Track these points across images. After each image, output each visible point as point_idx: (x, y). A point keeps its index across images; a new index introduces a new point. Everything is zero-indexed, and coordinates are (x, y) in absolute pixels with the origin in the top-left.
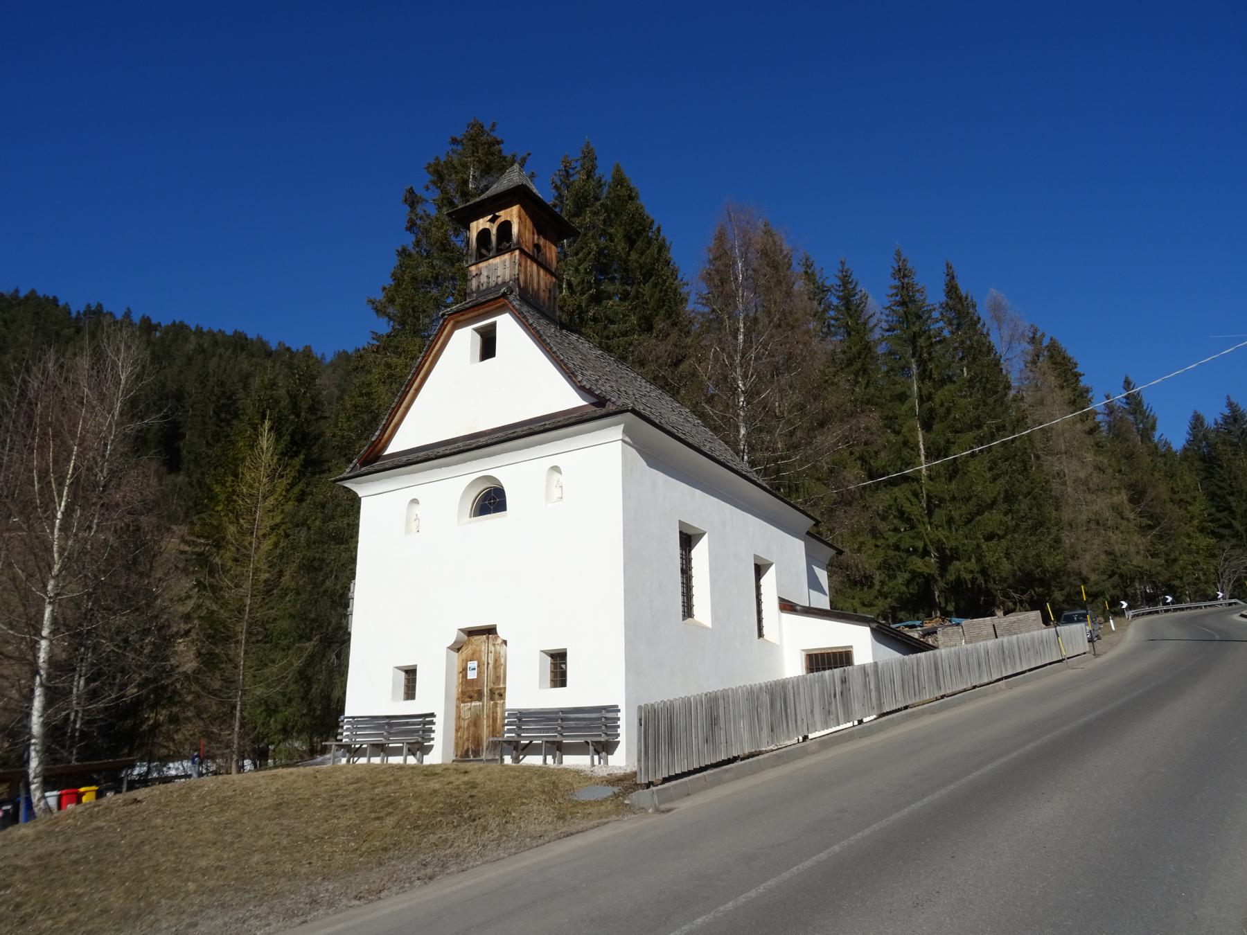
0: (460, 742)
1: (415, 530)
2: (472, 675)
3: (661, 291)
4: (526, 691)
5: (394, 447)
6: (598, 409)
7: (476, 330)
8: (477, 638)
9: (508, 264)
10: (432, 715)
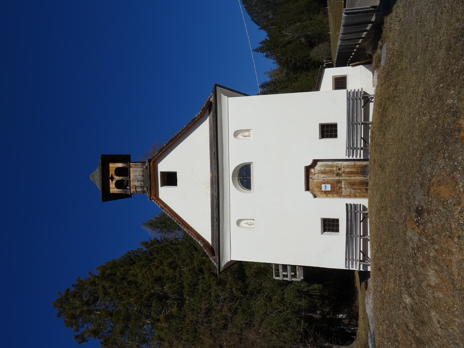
0: (362, 194)
1: (253, 221)
2: (329, 188)
3: (161, 250)
4: (336, 148)
5: (208, 237)
6: (212, 109)
8: (310, 186)
9: (135, 169)
10: (347, 205)
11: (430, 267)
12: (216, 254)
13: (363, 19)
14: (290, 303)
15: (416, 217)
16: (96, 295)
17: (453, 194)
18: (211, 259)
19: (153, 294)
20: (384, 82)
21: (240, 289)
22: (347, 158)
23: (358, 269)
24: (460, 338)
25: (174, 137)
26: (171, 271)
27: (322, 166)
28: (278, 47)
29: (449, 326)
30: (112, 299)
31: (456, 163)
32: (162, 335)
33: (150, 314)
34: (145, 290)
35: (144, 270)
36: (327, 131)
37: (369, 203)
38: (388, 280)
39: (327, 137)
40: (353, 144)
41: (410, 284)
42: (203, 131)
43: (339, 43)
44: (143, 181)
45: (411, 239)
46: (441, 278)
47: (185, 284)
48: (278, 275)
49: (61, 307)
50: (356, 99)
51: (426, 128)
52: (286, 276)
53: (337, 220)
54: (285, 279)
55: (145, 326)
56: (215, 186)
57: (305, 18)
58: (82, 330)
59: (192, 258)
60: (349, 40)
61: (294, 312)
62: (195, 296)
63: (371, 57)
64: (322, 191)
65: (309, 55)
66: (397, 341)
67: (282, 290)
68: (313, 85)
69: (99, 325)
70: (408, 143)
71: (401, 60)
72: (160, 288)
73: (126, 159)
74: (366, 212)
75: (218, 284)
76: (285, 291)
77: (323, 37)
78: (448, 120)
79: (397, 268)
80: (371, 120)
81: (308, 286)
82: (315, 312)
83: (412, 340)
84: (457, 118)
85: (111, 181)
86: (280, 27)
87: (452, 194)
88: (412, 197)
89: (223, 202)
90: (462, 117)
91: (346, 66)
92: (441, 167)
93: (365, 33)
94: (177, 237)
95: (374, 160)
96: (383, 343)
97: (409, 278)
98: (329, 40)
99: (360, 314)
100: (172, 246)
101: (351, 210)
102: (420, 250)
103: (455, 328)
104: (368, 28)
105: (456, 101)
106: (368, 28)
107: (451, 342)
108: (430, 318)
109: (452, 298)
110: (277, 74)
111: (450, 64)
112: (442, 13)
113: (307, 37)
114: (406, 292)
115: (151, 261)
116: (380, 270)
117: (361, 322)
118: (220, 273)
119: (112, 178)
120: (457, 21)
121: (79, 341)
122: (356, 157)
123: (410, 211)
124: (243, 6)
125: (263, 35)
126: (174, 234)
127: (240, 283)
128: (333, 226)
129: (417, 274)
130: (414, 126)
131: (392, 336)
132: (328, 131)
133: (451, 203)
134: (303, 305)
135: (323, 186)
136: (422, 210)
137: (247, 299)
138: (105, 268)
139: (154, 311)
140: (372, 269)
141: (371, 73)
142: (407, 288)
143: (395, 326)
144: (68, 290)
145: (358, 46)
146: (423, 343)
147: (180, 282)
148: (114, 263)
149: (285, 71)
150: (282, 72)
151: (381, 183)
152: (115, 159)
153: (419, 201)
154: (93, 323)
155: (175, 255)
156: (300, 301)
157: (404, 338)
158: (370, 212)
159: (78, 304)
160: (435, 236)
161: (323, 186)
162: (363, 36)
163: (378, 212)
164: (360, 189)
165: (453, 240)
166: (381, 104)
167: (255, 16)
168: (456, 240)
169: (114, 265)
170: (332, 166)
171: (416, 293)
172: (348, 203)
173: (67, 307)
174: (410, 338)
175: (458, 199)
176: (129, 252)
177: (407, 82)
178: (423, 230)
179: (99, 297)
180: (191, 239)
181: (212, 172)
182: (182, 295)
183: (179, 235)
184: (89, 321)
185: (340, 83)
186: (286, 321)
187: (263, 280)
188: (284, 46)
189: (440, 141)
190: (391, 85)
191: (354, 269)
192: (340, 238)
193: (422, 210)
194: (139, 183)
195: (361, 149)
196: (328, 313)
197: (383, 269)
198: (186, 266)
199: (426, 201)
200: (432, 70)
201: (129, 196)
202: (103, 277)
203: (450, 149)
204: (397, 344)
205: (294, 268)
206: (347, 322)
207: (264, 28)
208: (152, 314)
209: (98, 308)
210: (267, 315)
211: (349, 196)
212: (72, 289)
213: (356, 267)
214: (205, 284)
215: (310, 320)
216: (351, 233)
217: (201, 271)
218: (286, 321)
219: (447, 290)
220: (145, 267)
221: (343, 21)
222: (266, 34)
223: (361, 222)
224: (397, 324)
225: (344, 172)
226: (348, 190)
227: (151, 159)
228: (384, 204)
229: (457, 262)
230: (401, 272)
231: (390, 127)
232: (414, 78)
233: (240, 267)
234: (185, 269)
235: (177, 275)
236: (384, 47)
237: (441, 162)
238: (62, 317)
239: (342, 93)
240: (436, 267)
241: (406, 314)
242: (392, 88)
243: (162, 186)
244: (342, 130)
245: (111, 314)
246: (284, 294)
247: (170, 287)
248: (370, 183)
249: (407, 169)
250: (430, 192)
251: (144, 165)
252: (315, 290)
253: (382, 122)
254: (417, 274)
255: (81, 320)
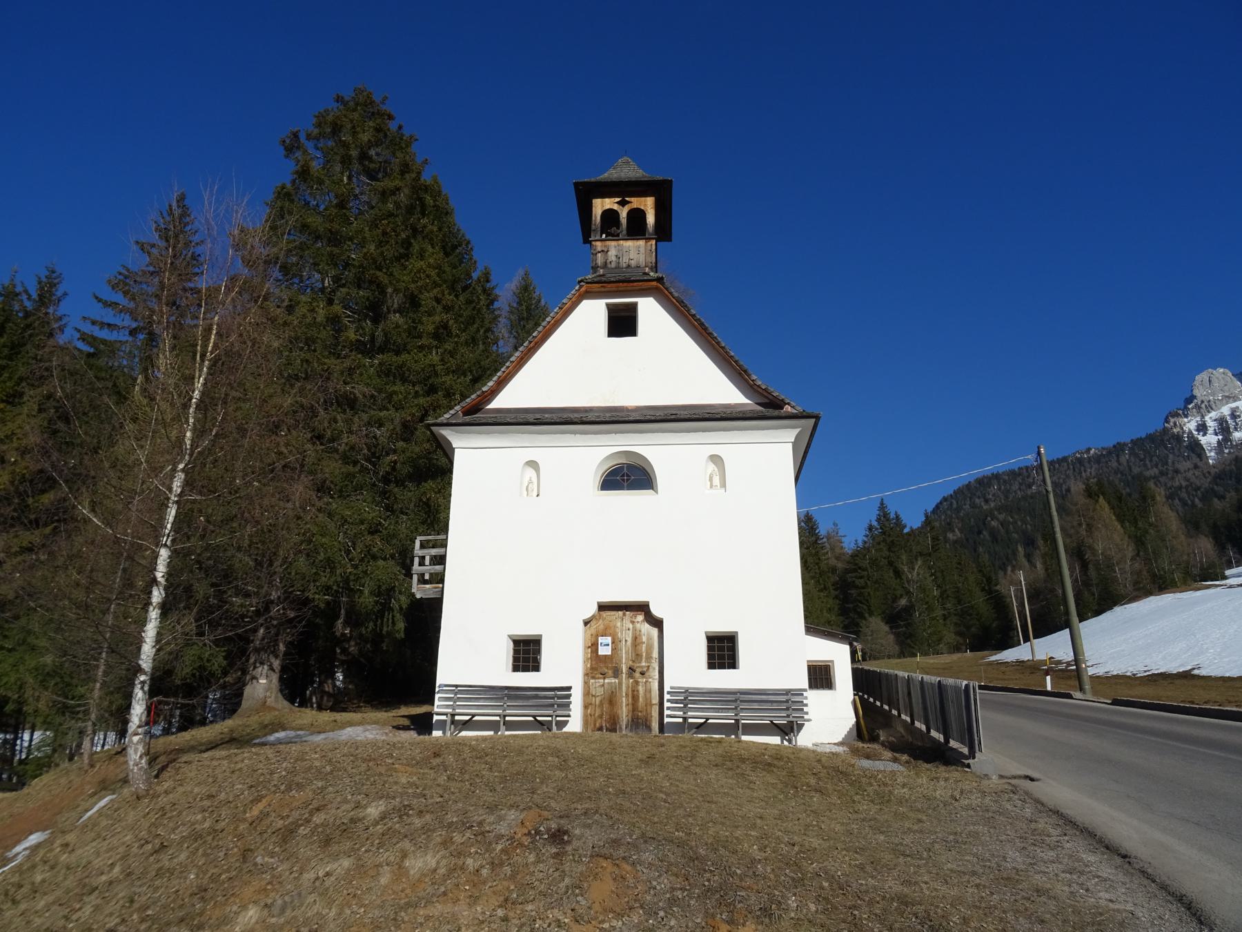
2: (604, 651)
3: (474, 309)
4: (686, 667)
6: (768, 408)
7: (608, 305)
9: (642, 250)
10: (569, 688)
11: (443, 857)
12: (468, 419)
13: (954, 725)
14: (365, 572)
15: (548, 830)
16: (380, 175)
17: (597, 907)
18: (458, 408)
19: (383, 292)
20: (823, 768)
21: (394, 469)
23: (436, 710)
24: (295, 917)
25: (711, 330)
26: (431, 328)
27: (650, 638)
28: (889, 550)
29: (320, 895)
30: (373, 208)
31: (662, 914)
32: (301, 310)
33: (343, 286)
34: (391, 274)
35: (433, 273)
36: (721, 649)
37: (574, 734)
38: (415, 770)
39: (710, 649)
40: (694, 702)
41: (408, 815)
42: (723, 391)
43: (903, 674)
44: (618, 267)
45: (501, 818)
46: (419, 880)
47: (405, 356)
48: (422, 546)
49: (357, 104)
50: (787, 709)
51: (735, 852)
52: (422, 564)
53: (537, 668)
54: (416, 560)
55: (317, 276)
56: (608, 415)
57: (948, 605)
58: (309, 146)
59: (459, 371)
60: (909, 694)
61: (347, 581)
62: (379, 376)
63: (874, 739)
64: (597, 636)
65: (871, 614)
66: (289, 789)
67: (392, 556)
68: (816, 624)
69: (321, 182)
70: (702, 814)
71: (872, 801)
72: (396, 306)
73: (663, 232)
74: (554, 727)
75: (405, 425)
76: (391, 562)
77: (908, 644)
78: (754, 898)
79: (439, 790)
80: (744, 738)
81: (401, 608)
82: (347, 623)
83: (290, 820)
84: (758, 917)
85: (618, 200)
86: (930, 555)
87: (597, 904)
88: (590, 821)
89: (575, 433)
90: (760, 927)
91: (855, 689)
92: (654, 883)
93: (924, 728)
94: (501, 343)
95: (662, 745)
96: (285, 759)
97: (420, 813)
98: (902, 655)
99: (343, 714)
100: (482, 331)
101: (558, 697)
102: (479, 838)
103: (316, 908)
104: (934, 733)
105: (793, 915)
106: (934, 733)
107: (287, 898)
108: (336, 857)
109: (379, 902)
110: (832, 549)
111: (871, 903)
112: (977, 886)
113: (909, 609)
114: (390, 807)
115: (452, 288)
116: (436, 755)
117: (326, 716)
118: (428, 426)
119: (623, 203)
120: (964, 918)
121: (288, 141)
122: (668, 708)
123: (561, 817)
124: (972, 480)
125: (913, 520)
126: (506, 335)
127: (406, 470)
128: (526, 660)
129: (427, 830)
130: (737, 827)
131: (298, 779)
132: (722, 650)
133: (578, 902)
134: (361, 600)
135: (609, 640)
136: (563, 842)
137: (374, 485)
138: (437, 194)
139: (348, 294)
140: (437, 739)
141: (840, 739)
142: (399, 810)
143: (320, 784)
144: (390, 117)
145: (895, 712)
146: (285, 840)
147: (408, 347)
148: (447, 213)
149: (840, 565)
150: (838, 558)
151: (616, 758)
152: (663, 210)
153: (582, 835)
154: (323, 168)
155: (464, 337)
156: (371, 593)
157: (295, 804)
158: (555, 736)
159: (361, 141)
160: (507, 870)
161: (609, 640)
162: (917, 724)
163: (556, 753)
164: (601, 717)
165: (500, 906)
166: (780, 759)
167: (951, 504)
168: (500, 912)
169: (442, 213)
170: (649, 658)
171: (389, 829)
172: (572, 691)
173: (356, 115)
174: (296, 814)
175: (586, 918)
176: (469, 242)
177: (828, 813)
178: (521, 845)
179: (378, 180)
180: (497, 370)
181: (638, 409)
182: (382, 350)
183: (503, 347)
184: (328, 161)
185: (820, 676)
186: (330, 564)
187: (412, 516)
188: (891, 564)
189: (709, 880)
190: (819, 779)
191: (437, 703)
193: (563, 842)
194: (614, 259)
195: (685, 719)
196: (344, 651)
197: (438, 760)
198: (442, 360)
199: (581, 851)
200: (856, 865)
201: (587, 240)
202: (419, 189)
203: (692, 902)
204: (283, 788)
205: (439, 579)
206: (328, 688)
207: (928, 521)
208: (344, 290)
209: (354, 180)
210: (343, 525)
211: (587, 693)
212: (393, 126)
213: (440, 706)
214: (405, 398)
215: (331, 612)
216: (510, 697)
217: (432, 390)
218: (330, 564)
219: (394, 892)
220: (438, 275)
221: (951, 681)
222: (915, 527)
223: (534, 717)
224: (323, 788)
225: (637, 683)
226: (600, 691)
227: (663, 284)
228: (572, 763)
229: (453, 915)
230: (432, 797)
231: (732, 778)
232: (838, 828)
233: (436, 470)
234: (435, 357)
235: (424, 341)
236: (896, 767)
237: (664, 883)
238: (336, 105)
239: (800, 680)
240: (442, 871)
241: (345, 807)
242: (813, 781)
243: (608, 305)
244: (723, 679)
245: (342, 205)
246: (385, 559)
247: (397, 326)
248: (614, 737)
249: (648, 811)
250: (601, 860)
251: (651, 269)
252: (394, 623)
253: (743, 760)
254: (429, 830)
255: (331, 143)
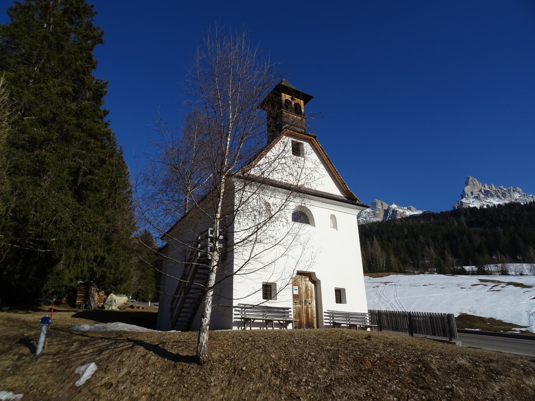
4: (329, 303)
6: (350, 199)
10: (288, 309)
22: (325, 309)
27: (311, 289)
40: (336, 317)
119: (292, 99)
132: (340, 295)
192: (258, 299)
248: (302, 330)
